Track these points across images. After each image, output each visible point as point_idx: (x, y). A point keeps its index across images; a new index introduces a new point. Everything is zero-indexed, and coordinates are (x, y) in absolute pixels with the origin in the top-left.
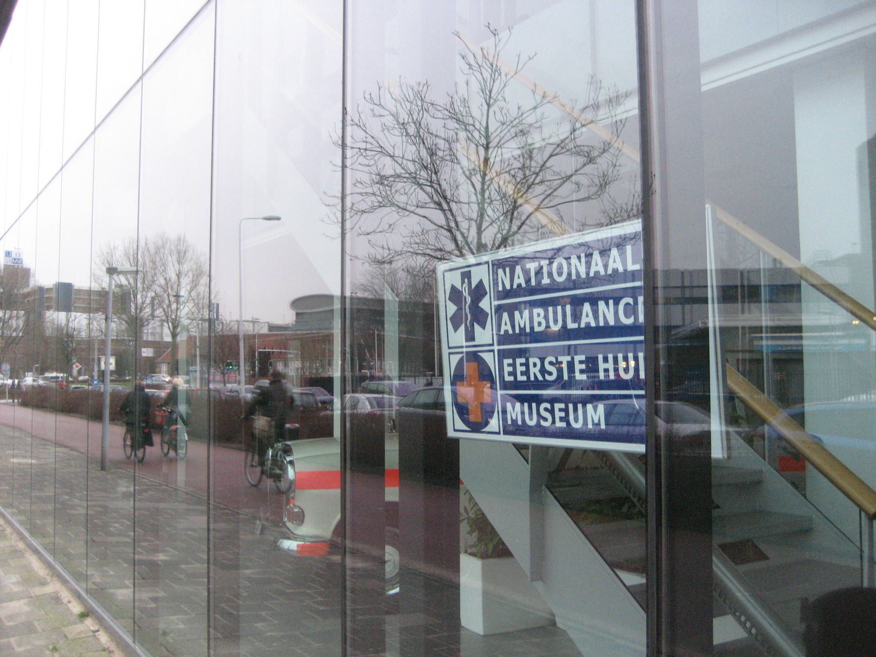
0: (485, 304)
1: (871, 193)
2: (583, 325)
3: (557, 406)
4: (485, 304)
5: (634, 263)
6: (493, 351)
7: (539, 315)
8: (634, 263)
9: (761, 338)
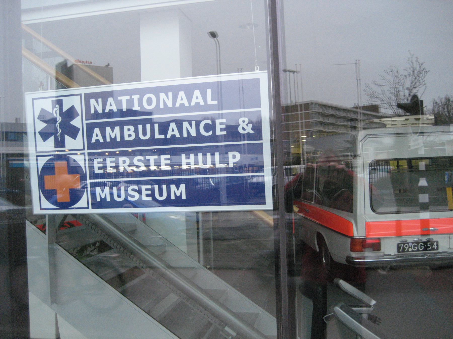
0: (76, 122)
1: (353, 182)
2: (169, 136)
3: (144, 187)
4: (76, 122)
5: (213, 100)
6: (84, 154)
7: (129, 130)
8: (213, 100)
9: (301, 114)
